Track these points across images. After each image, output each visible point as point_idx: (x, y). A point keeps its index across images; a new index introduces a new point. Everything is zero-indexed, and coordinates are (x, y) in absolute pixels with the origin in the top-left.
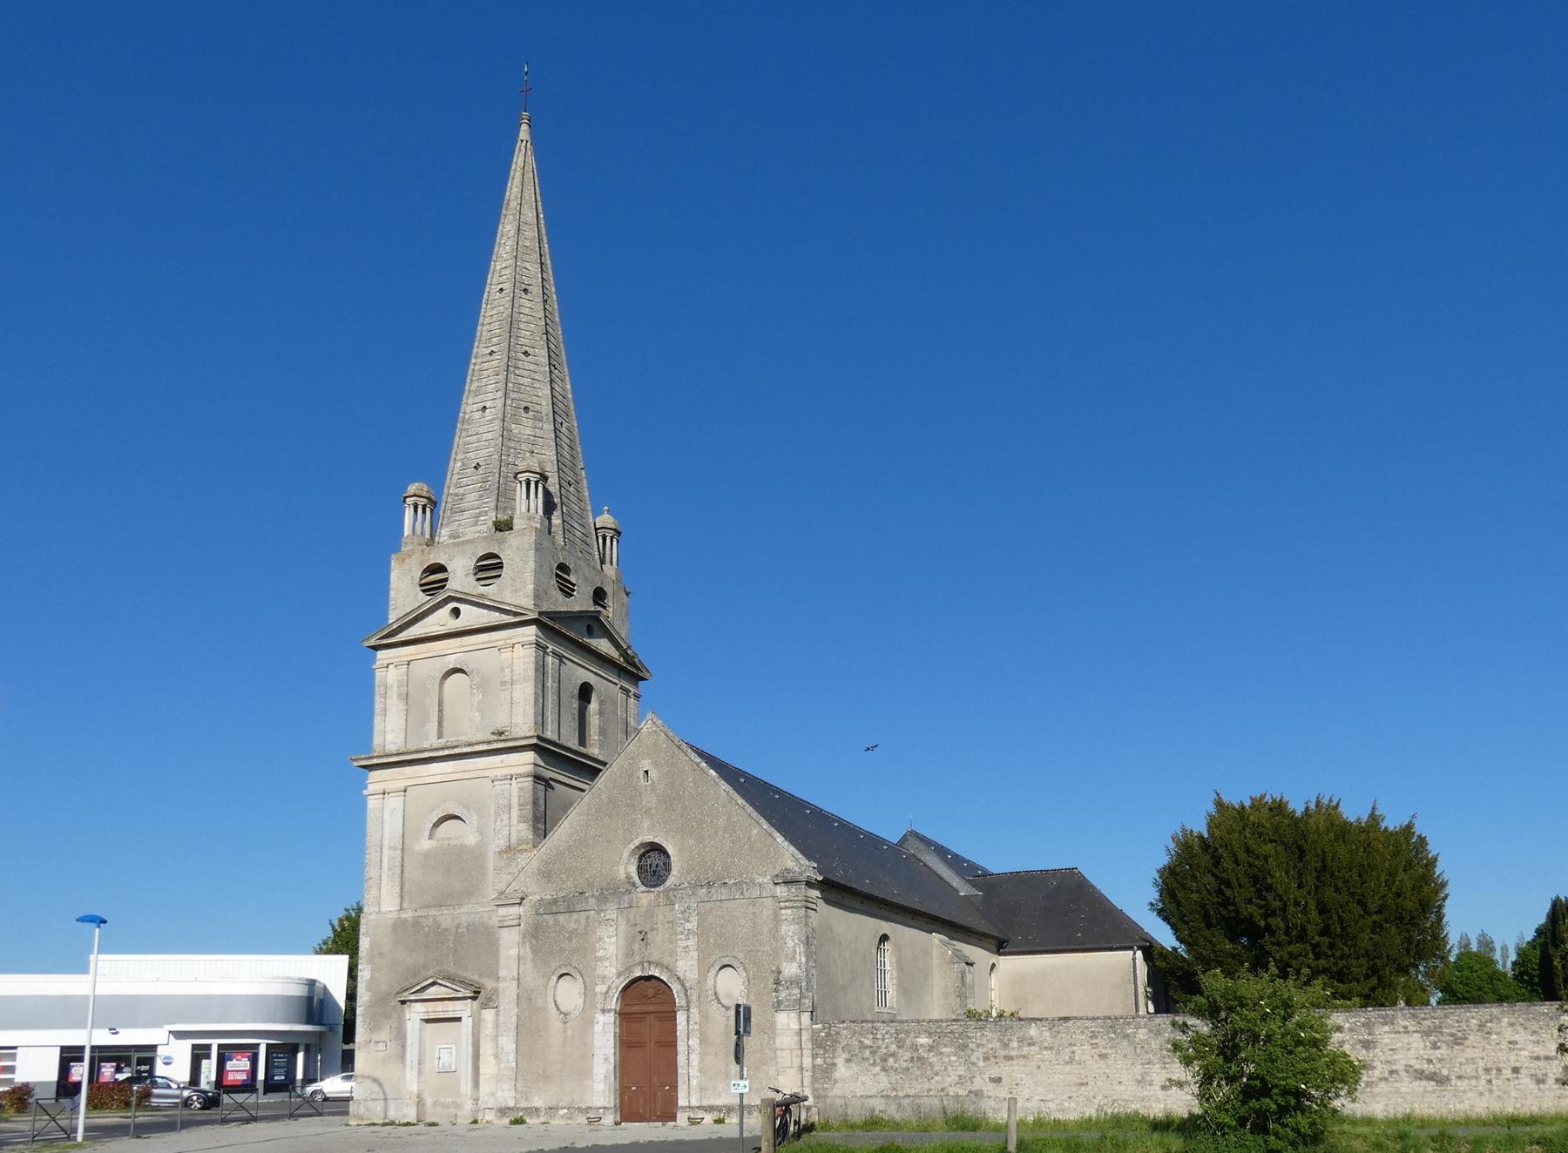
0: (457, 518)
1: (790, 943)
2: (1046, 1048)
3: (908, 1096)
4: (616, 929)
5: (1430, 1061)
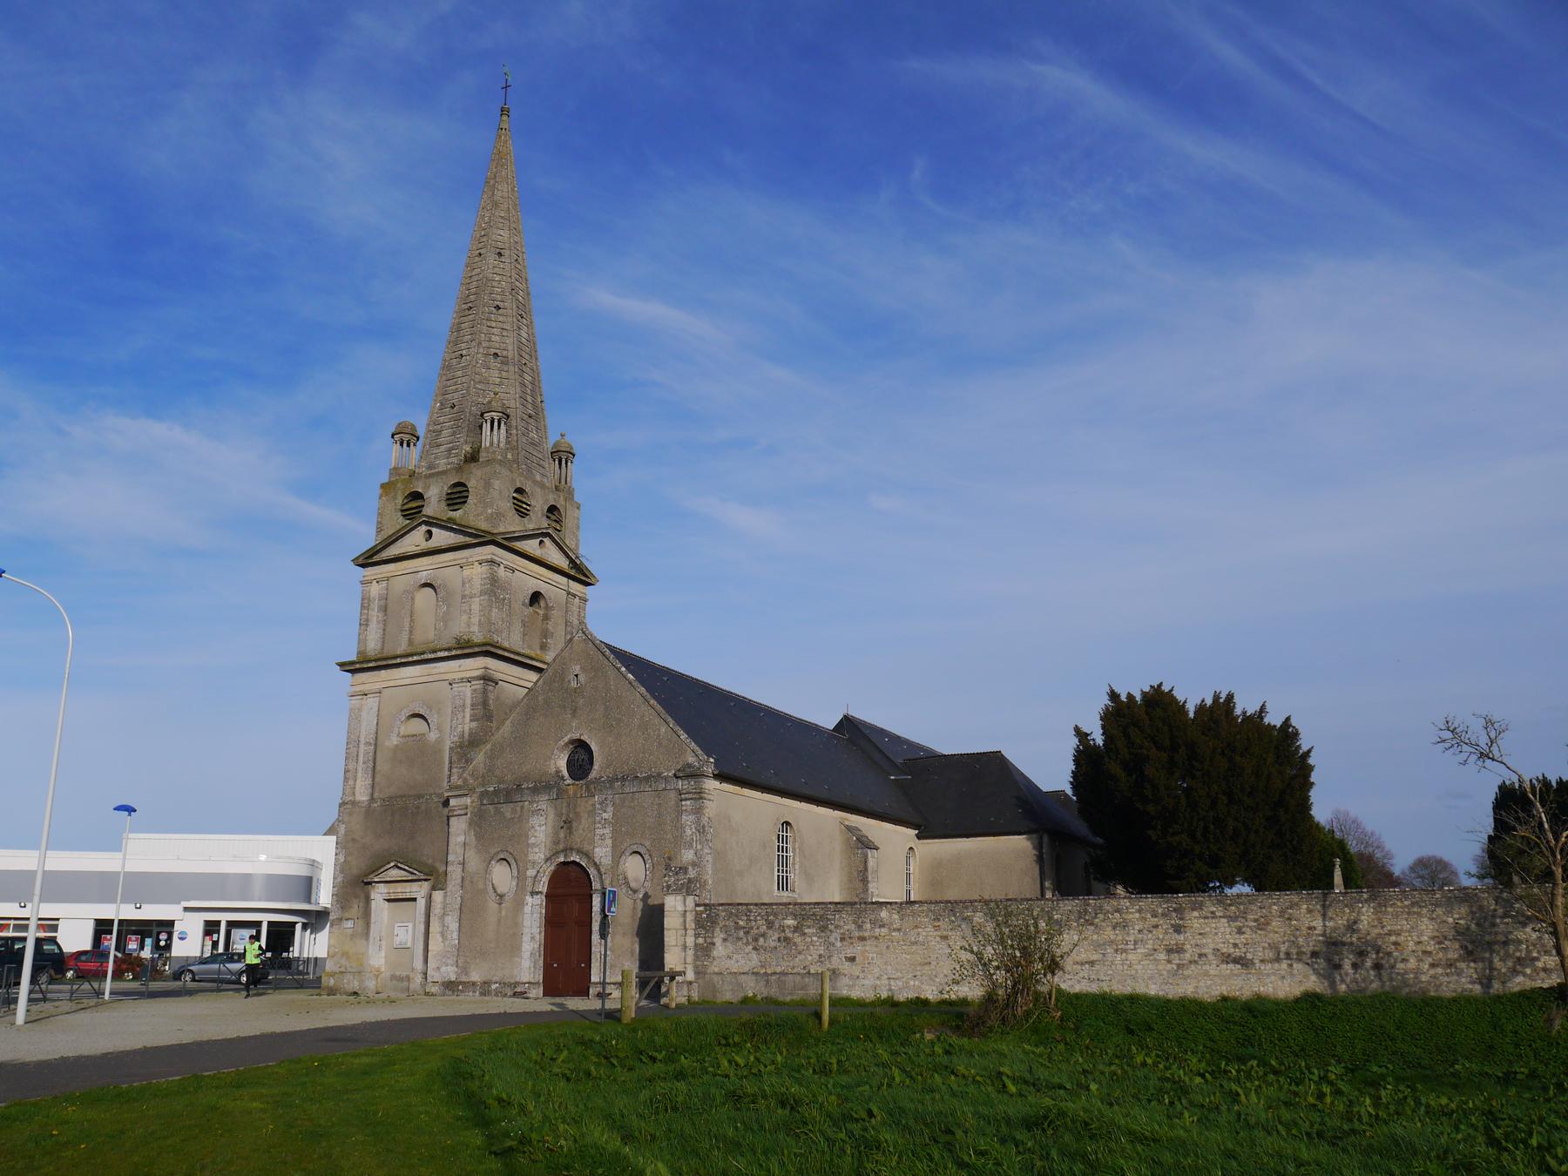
0: (435, 451)
1: (689, 832)
2: (894, 930)
3: (775, 973)
4: (546, 818)
5: (1235, 945)
